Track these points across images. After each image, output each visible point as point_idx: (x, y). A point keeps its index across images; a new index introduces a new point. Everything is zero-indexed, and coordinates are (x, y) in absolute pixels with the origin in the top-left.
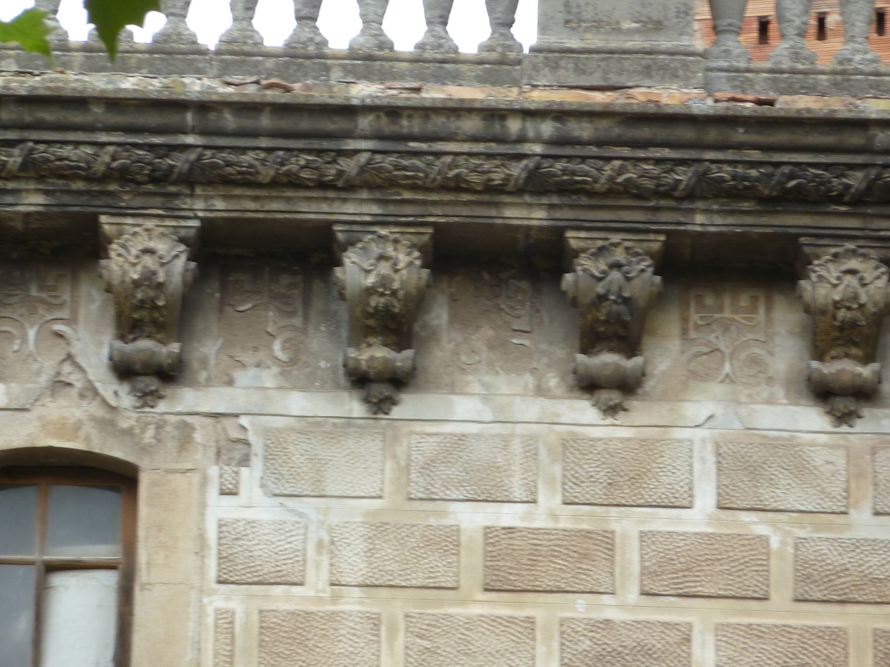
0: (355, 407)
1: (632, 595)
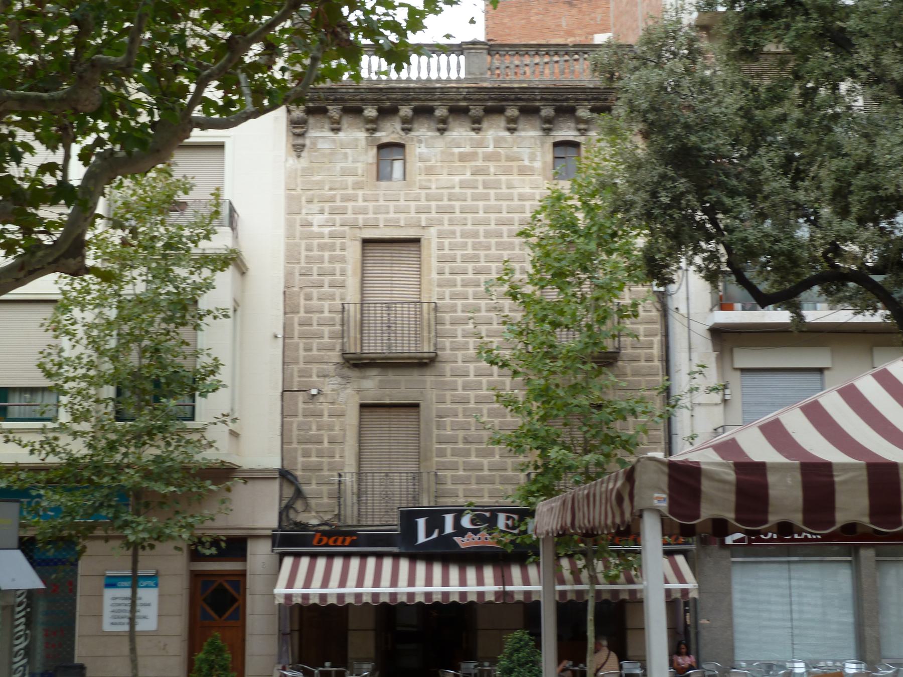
0: (438, 134)
1: (481, 161)
